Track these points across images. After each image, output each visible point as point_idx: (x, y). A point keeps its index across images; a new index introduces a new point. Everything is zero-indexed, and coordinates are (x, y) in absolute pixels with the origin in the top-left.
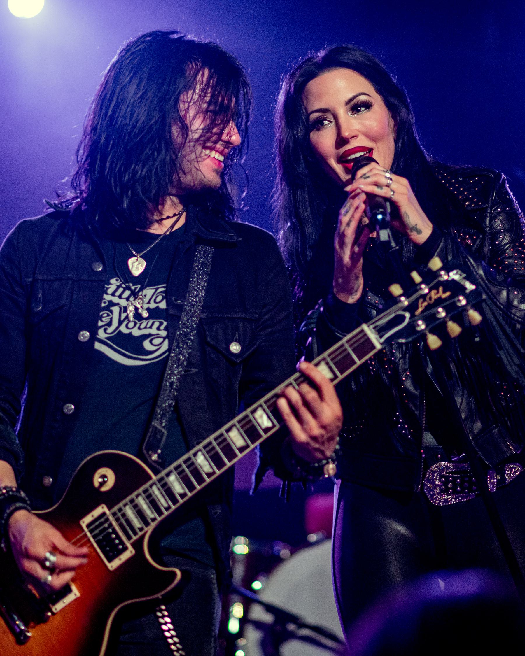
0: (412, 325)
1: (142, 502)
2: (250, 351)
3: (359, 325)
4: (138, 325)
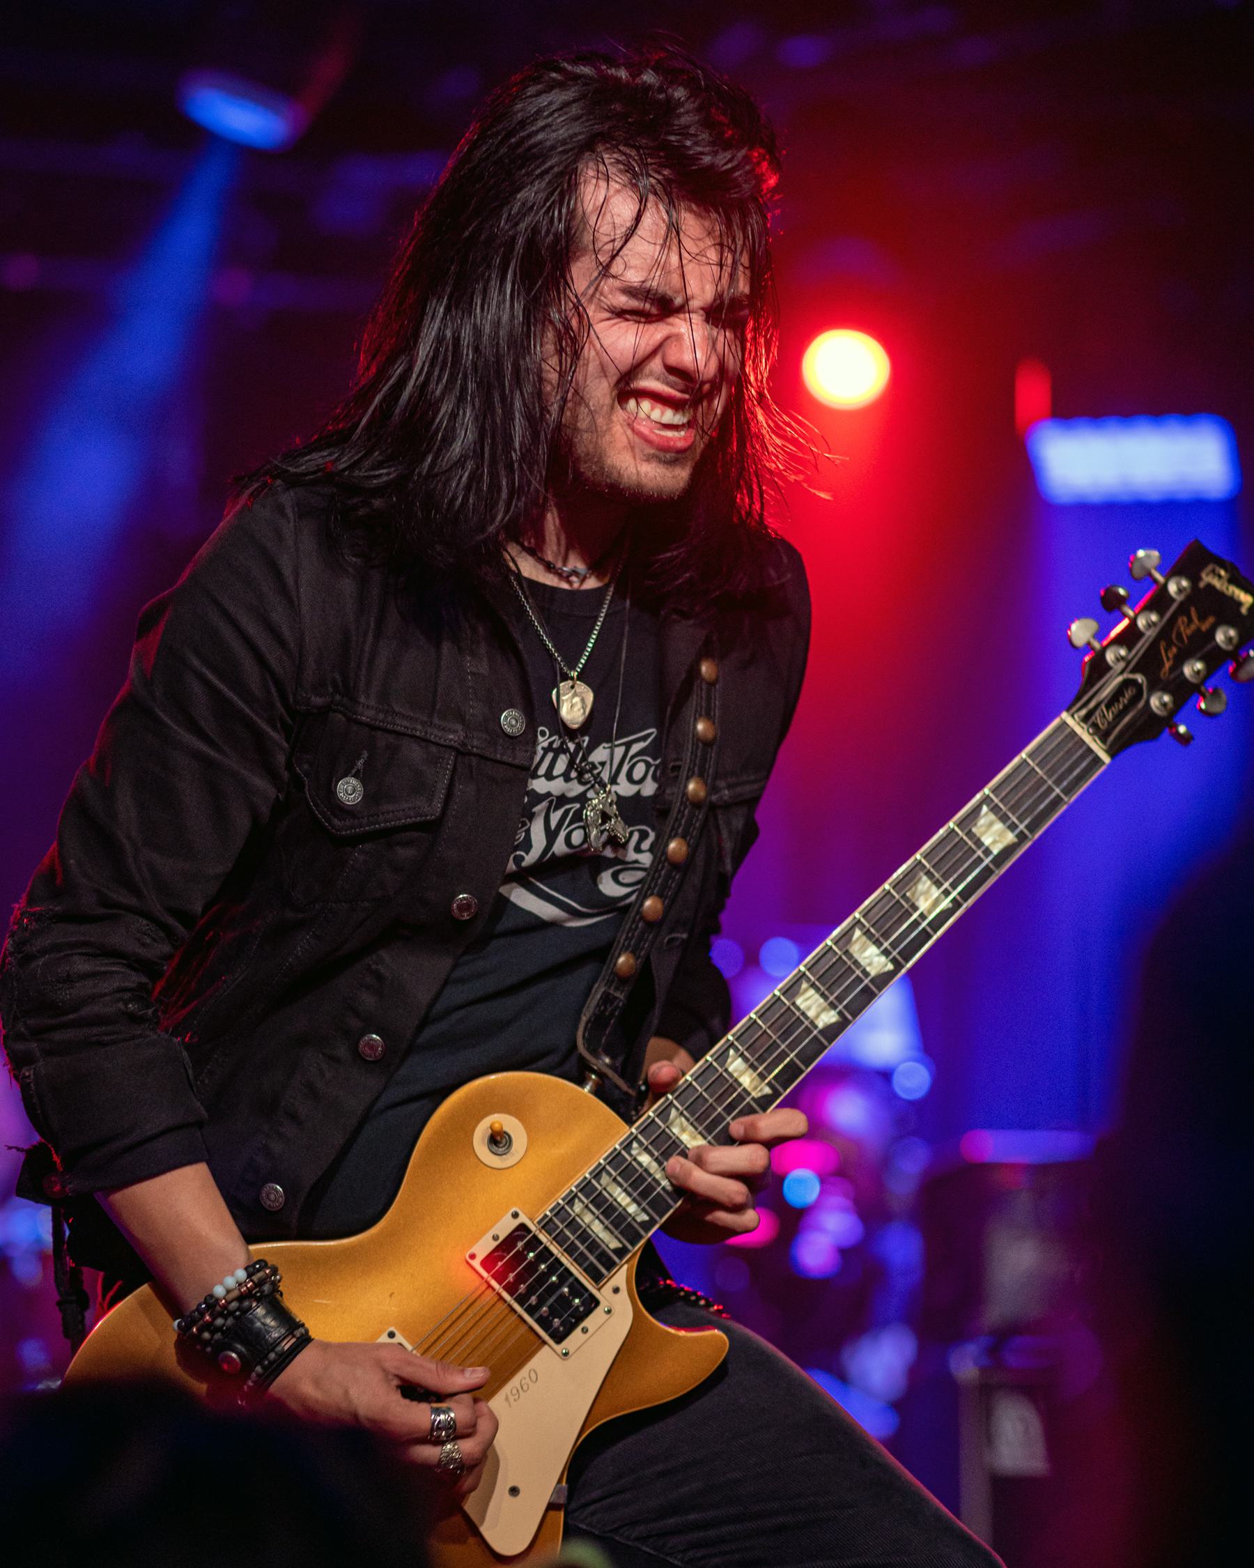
3: (1058, 714)
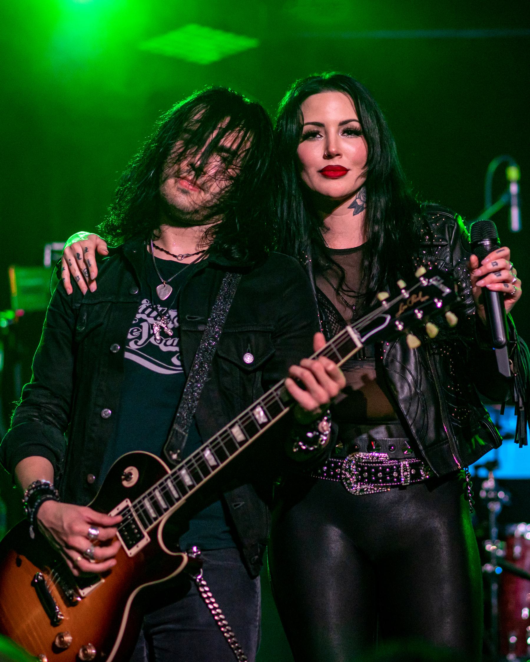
0: (392, 325)
1: (158, 495)
2: (178, 291)
4: (164, 341)
